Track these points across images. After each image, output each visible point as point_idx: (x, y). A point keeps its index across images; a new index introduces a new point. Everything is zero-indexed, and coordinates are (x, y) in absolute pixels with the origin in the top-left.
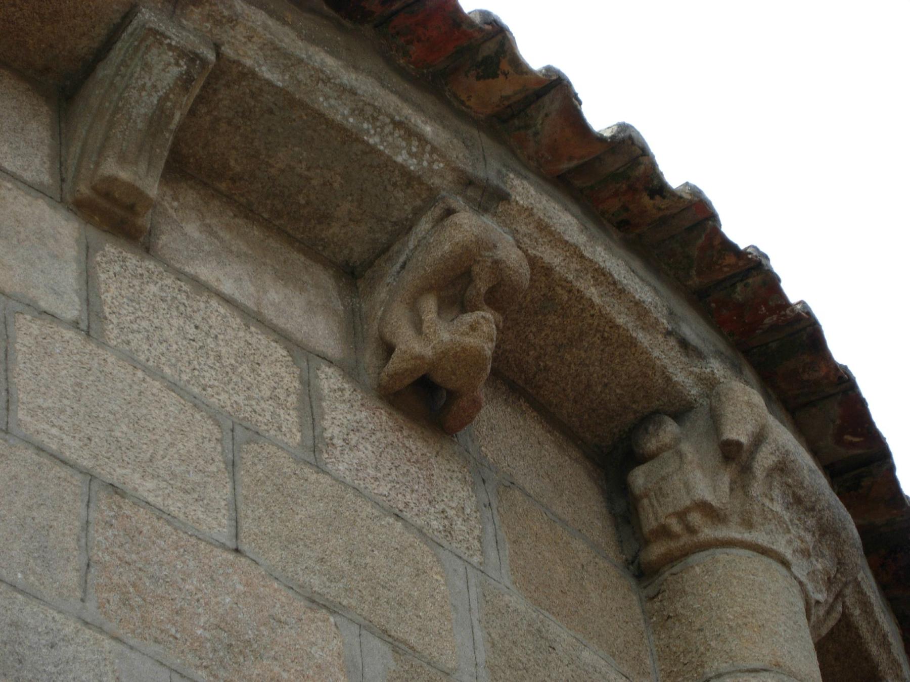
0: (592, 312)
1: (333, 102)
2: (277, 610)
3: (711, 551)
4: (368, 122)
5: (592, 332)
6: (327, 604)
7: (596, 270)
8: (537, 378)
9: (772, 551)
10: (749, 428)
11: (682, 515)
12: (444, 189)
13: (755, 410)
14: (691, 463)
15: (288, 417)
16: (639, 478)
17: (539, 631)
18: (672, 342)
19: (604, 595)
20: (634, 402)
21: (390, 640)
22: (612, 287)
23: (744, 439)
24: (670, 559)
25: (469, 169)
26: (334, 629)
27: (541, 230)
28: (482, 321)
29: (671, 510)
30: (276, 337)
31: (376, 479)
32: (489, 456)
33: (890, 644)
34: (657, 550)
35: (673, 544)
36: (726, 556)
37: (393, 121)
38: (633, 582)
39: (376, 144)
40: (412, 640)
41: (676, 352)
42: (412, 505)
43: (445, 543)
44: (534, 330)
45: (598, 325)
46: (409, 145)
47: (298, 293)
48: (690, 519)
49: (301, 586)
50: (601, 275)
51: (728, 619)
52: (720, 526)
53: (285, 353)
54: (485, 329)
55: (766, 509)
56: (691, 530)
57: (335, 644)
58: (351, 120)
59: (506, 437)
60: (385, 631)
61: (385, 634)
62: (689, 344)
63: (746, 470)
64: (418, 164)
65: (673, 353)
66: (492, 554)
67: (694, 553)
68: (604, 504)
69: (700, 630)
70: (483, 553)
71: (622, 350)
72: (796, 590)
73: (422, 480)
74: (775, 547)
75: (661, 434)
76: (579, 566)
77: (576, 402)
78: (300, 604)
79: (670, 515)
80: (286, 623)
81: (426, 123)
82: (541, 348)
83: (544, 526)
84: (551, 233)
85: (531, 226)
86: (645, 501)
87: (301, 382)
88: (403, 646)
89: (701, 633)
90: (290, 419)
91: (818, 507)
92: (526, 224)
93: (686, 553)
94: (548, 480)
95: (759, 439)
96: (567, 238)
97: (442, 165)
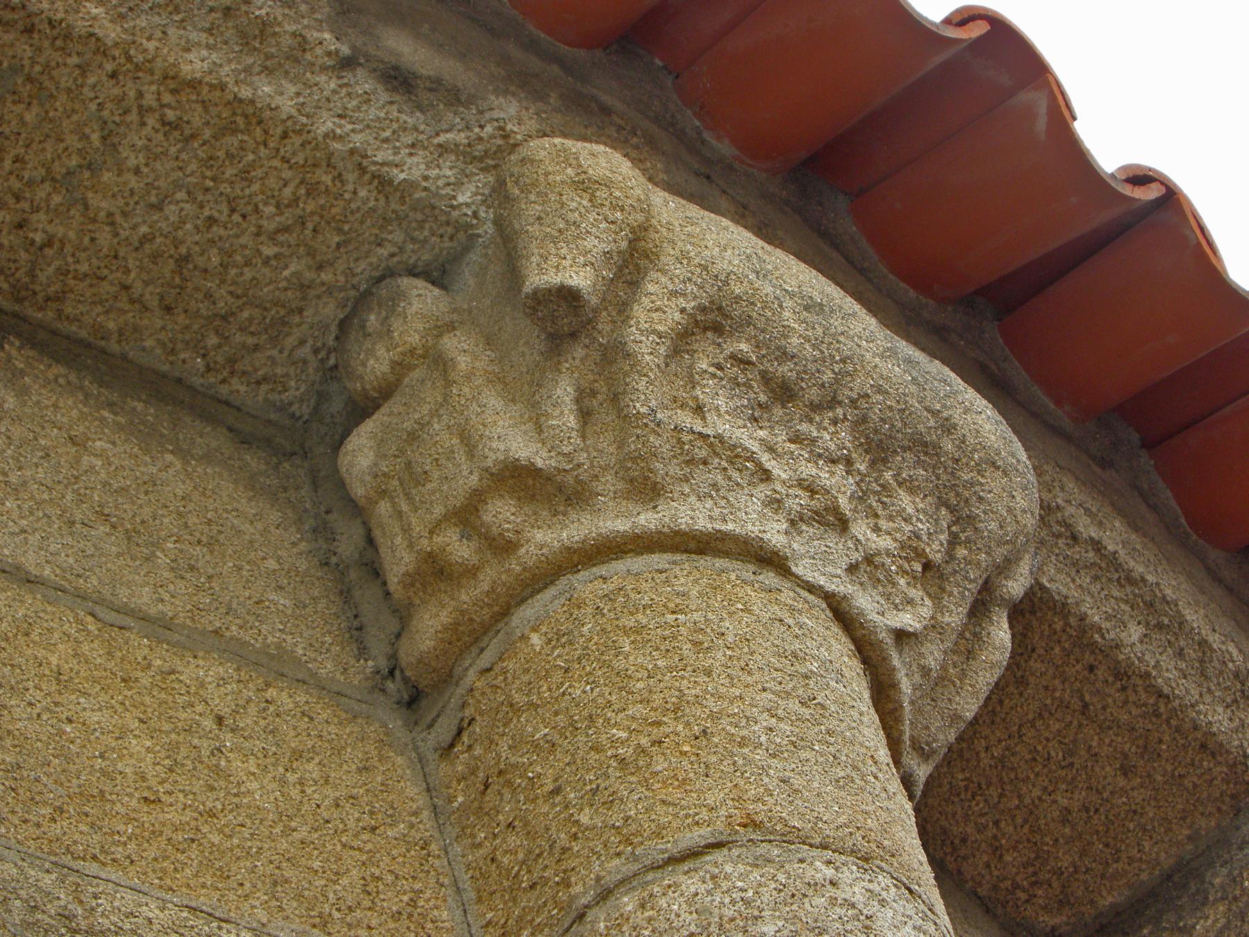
0: (109, 67)
3: (563, 582)
5: (133, 117)
8: (42, 277)
9: (723, 537)
10: (596, 245)
11: (466, 516)
13: (602, 194)
14: (468, 378)
16: (361, 454)
18: (364, 82)
19: (292, 778)
20: (320, 268)
23: (580, 279)
24: (469, 636)
29: (438, 510)
34: (430, 626)
36: (598, 584)
38: (395, 723)
41: (381, 105)
45: (140, 95)
48: (487, 518)
51: (614, 741)
52: (573, 516)
55: (686, 438)
56: (503, 547)
62: (416, 76)
63: (614, 356)
65: (373, 113)
69: (557, 791)
71: (232, 141)
72: (818, 622)
75: (397, 324)
76: (208, 723)
77: (168, 309)
79: (438, 524)
83: (85, 648)
86: (384, 508)
89: (558, 799)
91: (845, 394)
93: (505, 606)
94: (104, 529)
95: (633, 261)
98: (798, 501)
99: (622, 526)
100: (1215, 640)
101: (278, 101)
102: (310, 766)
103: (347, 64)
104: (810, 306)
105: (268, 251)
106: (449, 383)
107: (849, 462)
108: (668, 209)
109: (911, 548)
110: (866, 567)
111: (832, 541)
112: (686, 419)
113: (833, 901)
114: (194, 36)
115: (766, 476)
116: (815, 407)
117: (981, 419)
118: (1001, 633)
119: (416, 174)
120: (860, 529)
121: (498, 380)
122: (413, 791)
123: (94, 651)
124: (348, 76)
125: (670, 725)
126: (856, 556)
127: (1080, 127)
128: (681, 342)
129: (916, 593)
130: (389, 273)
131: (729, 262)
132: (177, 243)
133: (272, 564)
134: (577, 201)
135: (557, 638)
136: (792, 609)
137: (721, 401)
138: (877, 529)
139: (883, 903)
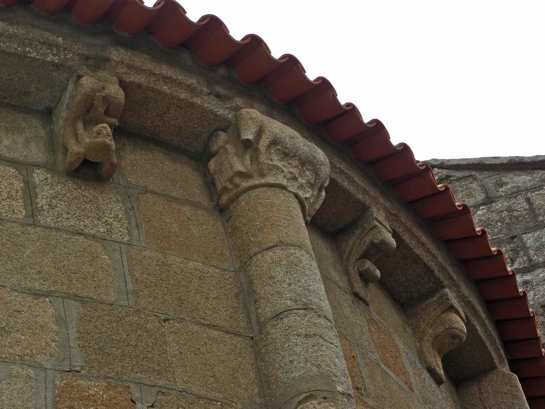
1: (8, 44)
2: (18, 307)
3: (248, 192)
4: (28, 47)
5: (172, 105)
6: (44, 293)
7: (163, 78)
10: (253, 130)
11: (231, 180)
12: (75, 66)
15: (18, 204)
16: (212, 165)
17: (163, 262)
18: (212, 97)
20: (204, 128)
21: (80, 299)
22: (174, 83)
23: (251, 137)
25: (86, 52)
26: (49, 304)
27: (130, 69)
28: (102, 129)
29: (226, 179)
30: (9, 164)
31: (68, 219)
32: (133, 181)
33: (368, 191)
34: (224, 199)
35: (231, 194)
37: (40, 43)
39: (35, 56)
40: (91, 295)
42: (89, 224)
43: (108, 238)
44: (145, 112)
46: (52, 51)
47: (20, 136)
49: (29, 290)
50: (166, 79)
51: (257, 225)
53: (14, 170)
54: (104, 132)
56: (237, 186)
57: (51, 311)
58: (19, 49)
59: (142, 167)
60: (76, 296)
61: (76, 297)
63: (256, 151)
64: (59, 58)
66: (135, 233)
67: (240, 195)
68: (202, 179)
69: (247, 233)
70: (129, 234)
71: (189, 109)
73: (93, 210)
74: (277, 182)
75: (218, 141)
76: (186, 219)
78: (29, 298)
80: (22, 311)
81: (57, 37)
82: (152, 118)
84: (136, 68)
85: (125, 68)
86: (216, 176)
87: (24, 183)
88: (86, 299)
90: (19, 205)
91: (297, 154)
92: (122, 68)
95: (260, 133)
96: (144, 68)
97: (71, 55)
98: (289, 176)
99: (257, 182)
100: (360, 183)
101: (197, 102)
102: (204, 226)
103: (209, 94)
104: (291, 138)
105: (195, 126)
106: (227, 155)
107: (298, 167)
108: (267, 120)
109: (308, 182)
110: (301, 187)
111: (295, 183)
112: (269, 162)
113: (295, 257)
114: (183, 91)
115: (283, 171)
116: (292, 157)
117: (321, 155)
118: (324, 194)
119: (221, 113)
120: (300, 180)
121: (236, 154)
122: (222, 229)
123: (166, 207)
124: (210, 96)
125: (267, 222)
126: (299, 185)
127: (338, 97)
128: (269, 147)
129: (309, 190)
130: (217, 130)
131: (277, 131)
132: (179, 125)
133: (196, 184)
134: (250, 122)
135: (247, 203)
136: (288, 197)
137: (275, 158)
138: (302, 179)
139: (303, 256)
